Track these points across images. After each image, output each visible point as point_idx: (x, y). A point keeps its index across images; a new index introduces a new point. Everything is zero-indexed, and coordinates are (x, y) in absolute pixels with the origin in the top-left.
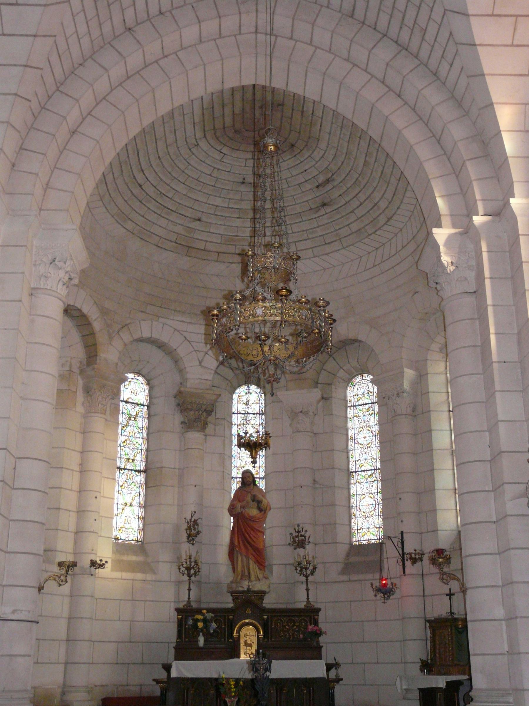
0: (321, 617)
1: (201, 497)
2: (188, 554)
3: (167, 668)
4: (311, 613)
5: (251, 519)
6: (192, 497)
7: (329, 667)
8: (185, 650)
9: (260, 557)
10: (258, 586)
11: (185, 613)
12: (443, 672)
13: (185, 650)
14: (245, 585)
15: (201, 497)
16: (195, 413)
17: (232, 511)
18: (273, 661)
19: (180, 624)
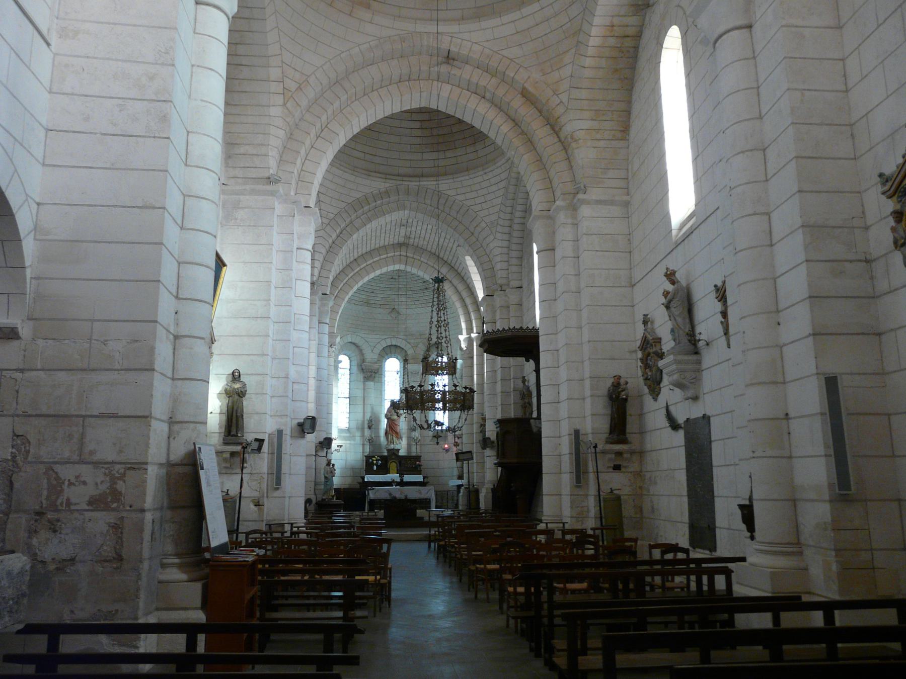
0: (422, 459)
1: (372, 409)
2: (368, 417)
3: (363, 478)
4: (418, 458)
5: (393, 420)
6: (368, 410)
7: (424, 478)
8: (369, 470)
9: (398, 436)
10: (397, 447)
11: (368, 458)
12: (309, 508)
13: (369, 470)
14: (392, 446)
15: (372, 409)
16: (369, 373)
17: (386, 416)
18: (185, 636)
19: (367, 461)
